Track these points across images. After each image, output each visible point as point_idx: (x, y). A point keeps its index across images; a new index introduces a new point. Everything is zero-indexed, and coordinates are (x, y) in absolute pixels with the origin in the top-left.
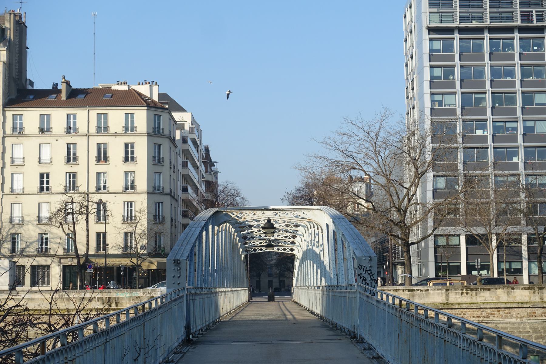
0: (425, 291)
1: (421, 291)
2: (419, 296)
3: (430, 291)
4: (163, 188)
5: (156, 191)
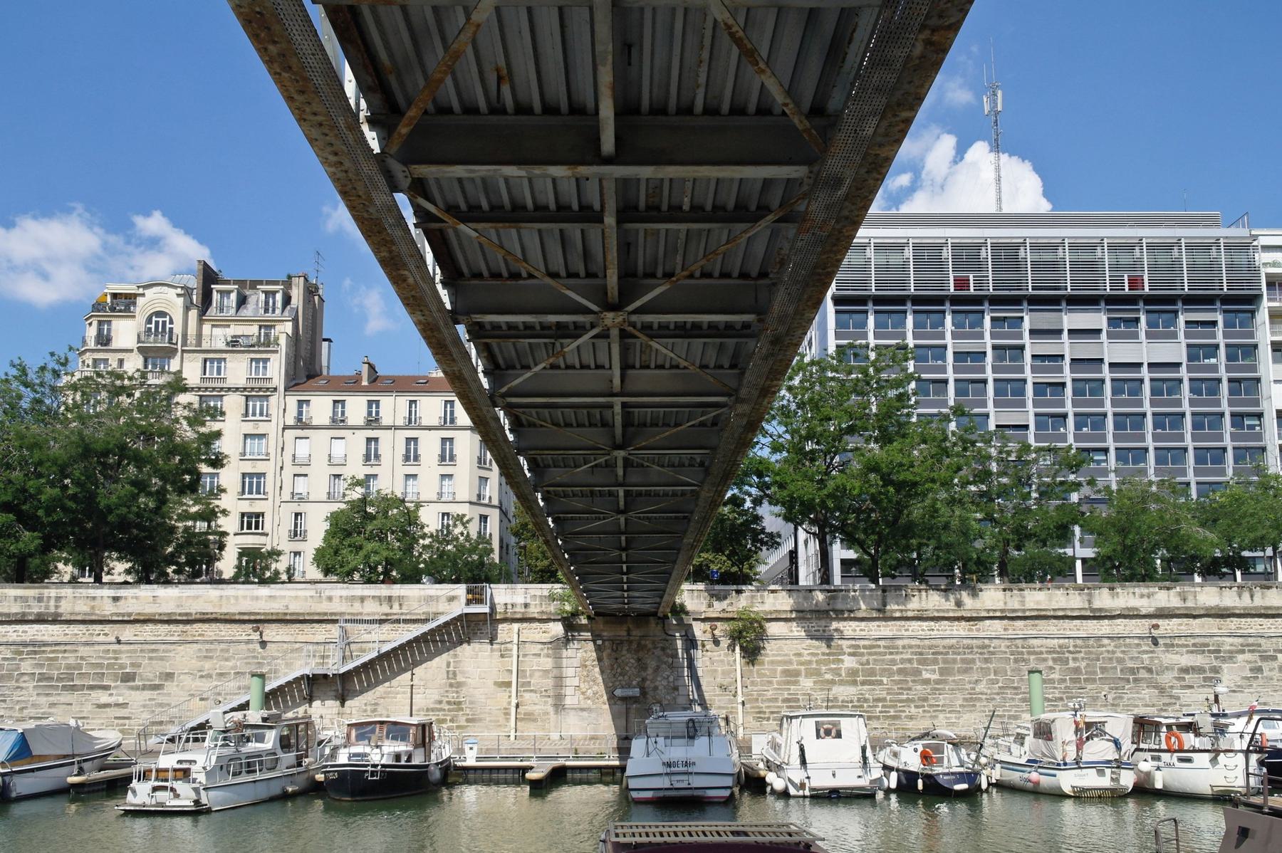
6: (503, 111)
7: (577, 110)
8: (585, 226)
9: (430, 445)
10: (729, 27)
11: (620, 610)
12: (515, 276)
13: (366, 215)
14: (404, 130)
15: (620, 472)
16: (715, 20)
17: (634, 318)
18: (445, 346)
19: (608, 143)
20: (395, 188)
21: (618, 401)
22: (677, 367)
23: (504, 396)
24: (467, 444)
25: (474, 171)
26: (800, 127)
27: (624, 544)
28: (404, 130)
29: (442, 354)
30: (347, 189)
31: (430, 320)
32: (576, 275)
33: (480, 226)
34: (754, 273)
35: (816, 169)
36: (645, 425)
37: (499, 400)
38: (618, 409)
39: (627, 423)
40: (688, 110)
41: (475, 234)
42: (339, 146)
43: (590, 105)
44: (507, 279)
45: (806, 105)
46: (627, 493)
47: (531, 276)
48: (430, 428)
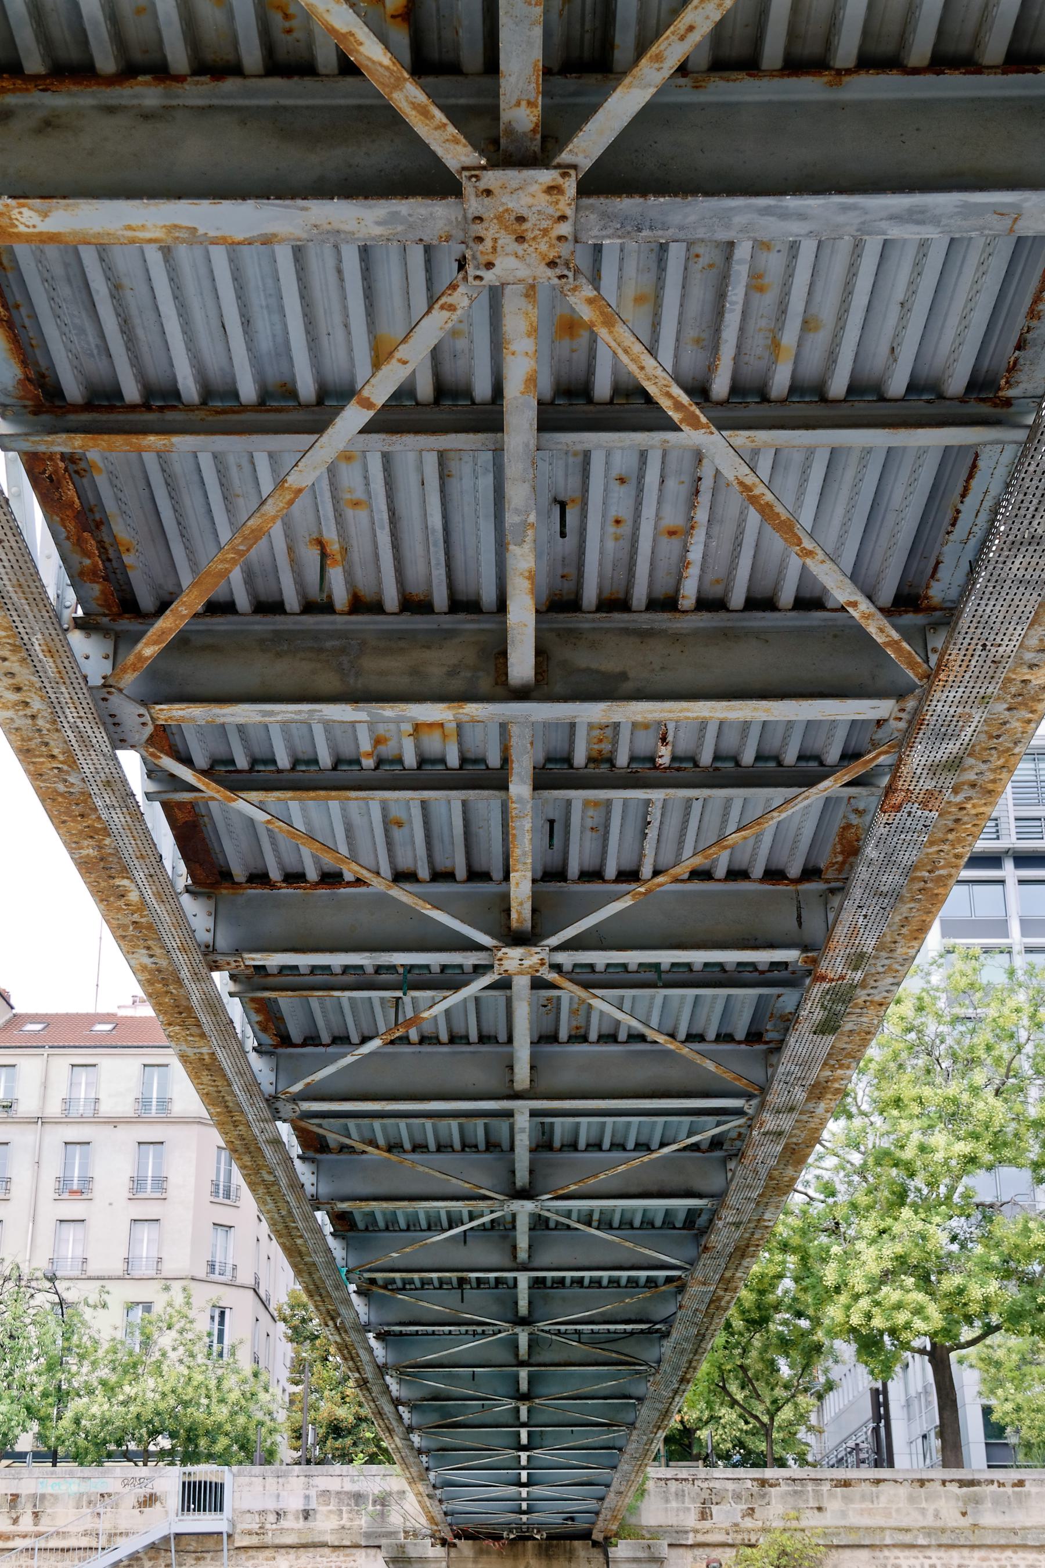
0: (1014, 1485)
1: (1001, 1485)
2: (996, 1501)
3: (1028, 1487)
4: (235, 1267)
5: (216, 1277)
6: (327, 607)
7: (462, 604)
8: (471, 794)
9: (113, 1163)
10: (746, 488)
11: (508, 1526)
12: (331, 878)
13: (61, 787)
14: (148, 650)
15: (523, 1241)
16: (717, 472)
17: (561, 958)
18: (189, 1009)
19: (522, 665)
20: (121, 742)
21: (522, 1108)
22: (642, 1038)
23: (295, 1099)
24: (196, 1153)
25: (271, 713)
26: (880, 639)
27: (524, 1387)
28: (148, 650)
29: (183, 1024)
30: (32, 744)
31: (164, 963)
32: (448, 876)
33: (271, 797)
34: (794, 871)
35: (911, 704)
36: (574, 1146)
37: (286, 1109)
38: (522, 1121)
39: (543, 1145)
40: (668, 603)
41: (260, 816)
42: (24, 675)
43: (488, 596)
44: (316, 885)
45: (887, 594)
46: (537, 1284)
47: (359, 882)
48: (114, 1122)
